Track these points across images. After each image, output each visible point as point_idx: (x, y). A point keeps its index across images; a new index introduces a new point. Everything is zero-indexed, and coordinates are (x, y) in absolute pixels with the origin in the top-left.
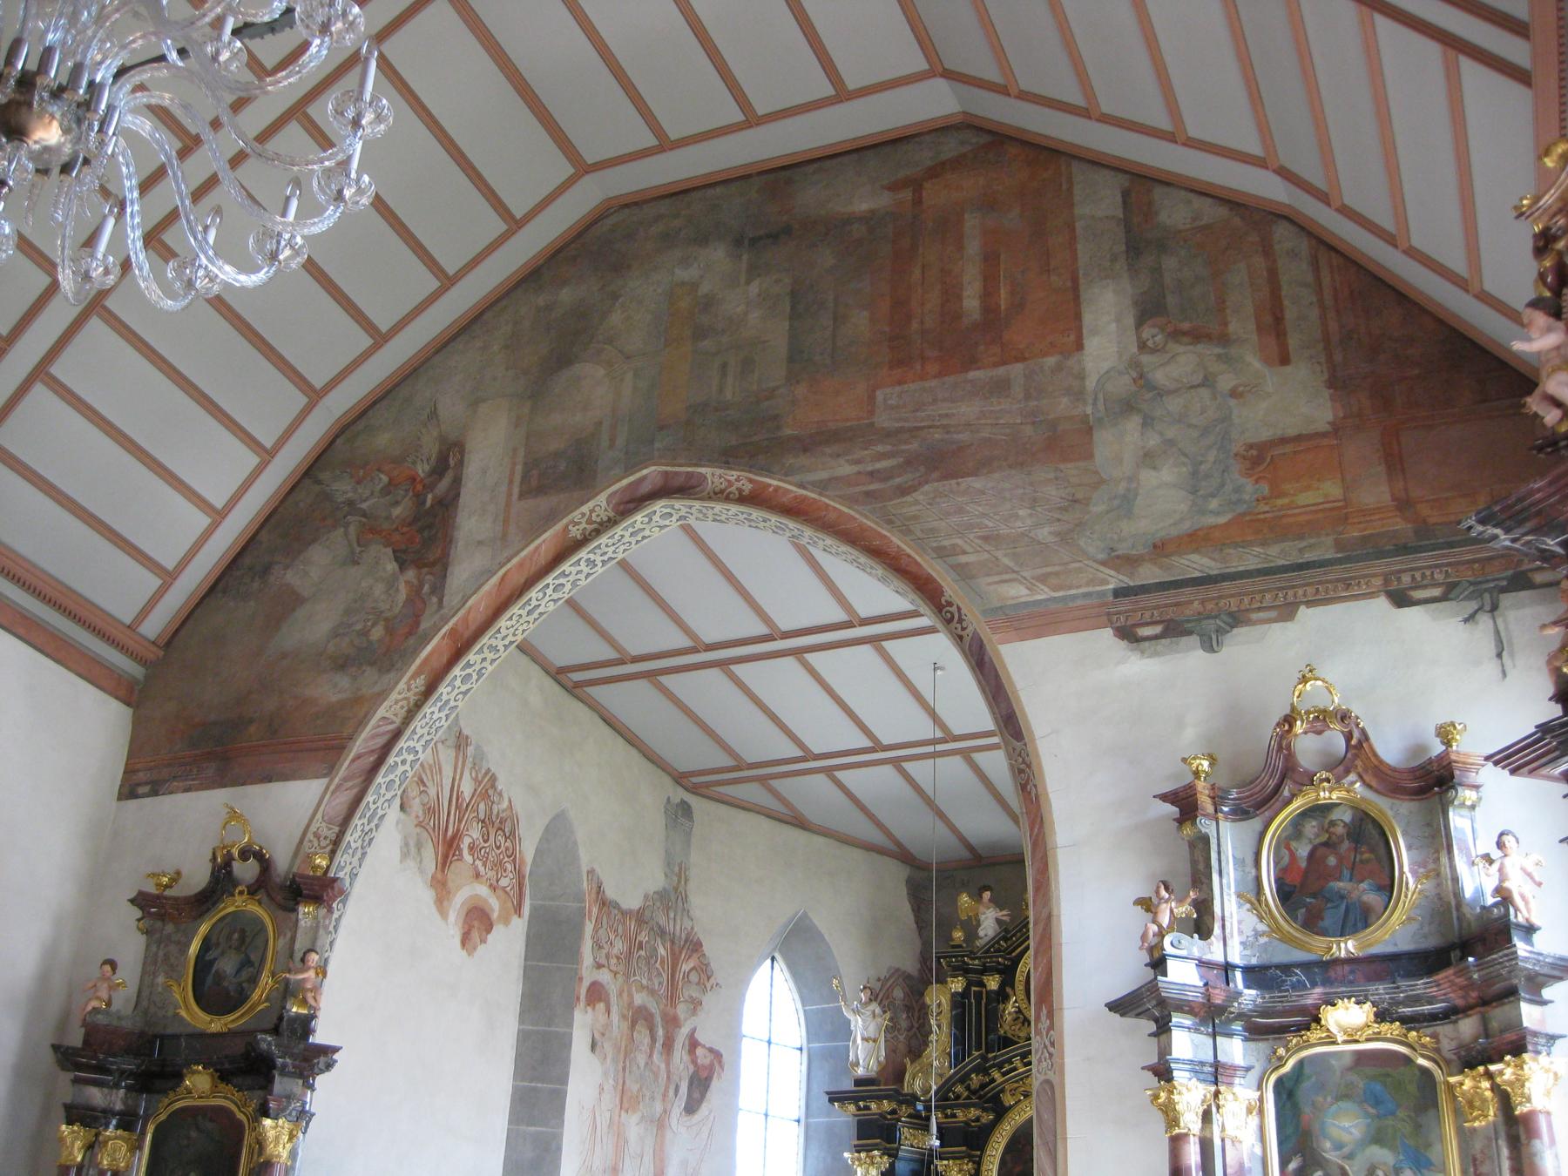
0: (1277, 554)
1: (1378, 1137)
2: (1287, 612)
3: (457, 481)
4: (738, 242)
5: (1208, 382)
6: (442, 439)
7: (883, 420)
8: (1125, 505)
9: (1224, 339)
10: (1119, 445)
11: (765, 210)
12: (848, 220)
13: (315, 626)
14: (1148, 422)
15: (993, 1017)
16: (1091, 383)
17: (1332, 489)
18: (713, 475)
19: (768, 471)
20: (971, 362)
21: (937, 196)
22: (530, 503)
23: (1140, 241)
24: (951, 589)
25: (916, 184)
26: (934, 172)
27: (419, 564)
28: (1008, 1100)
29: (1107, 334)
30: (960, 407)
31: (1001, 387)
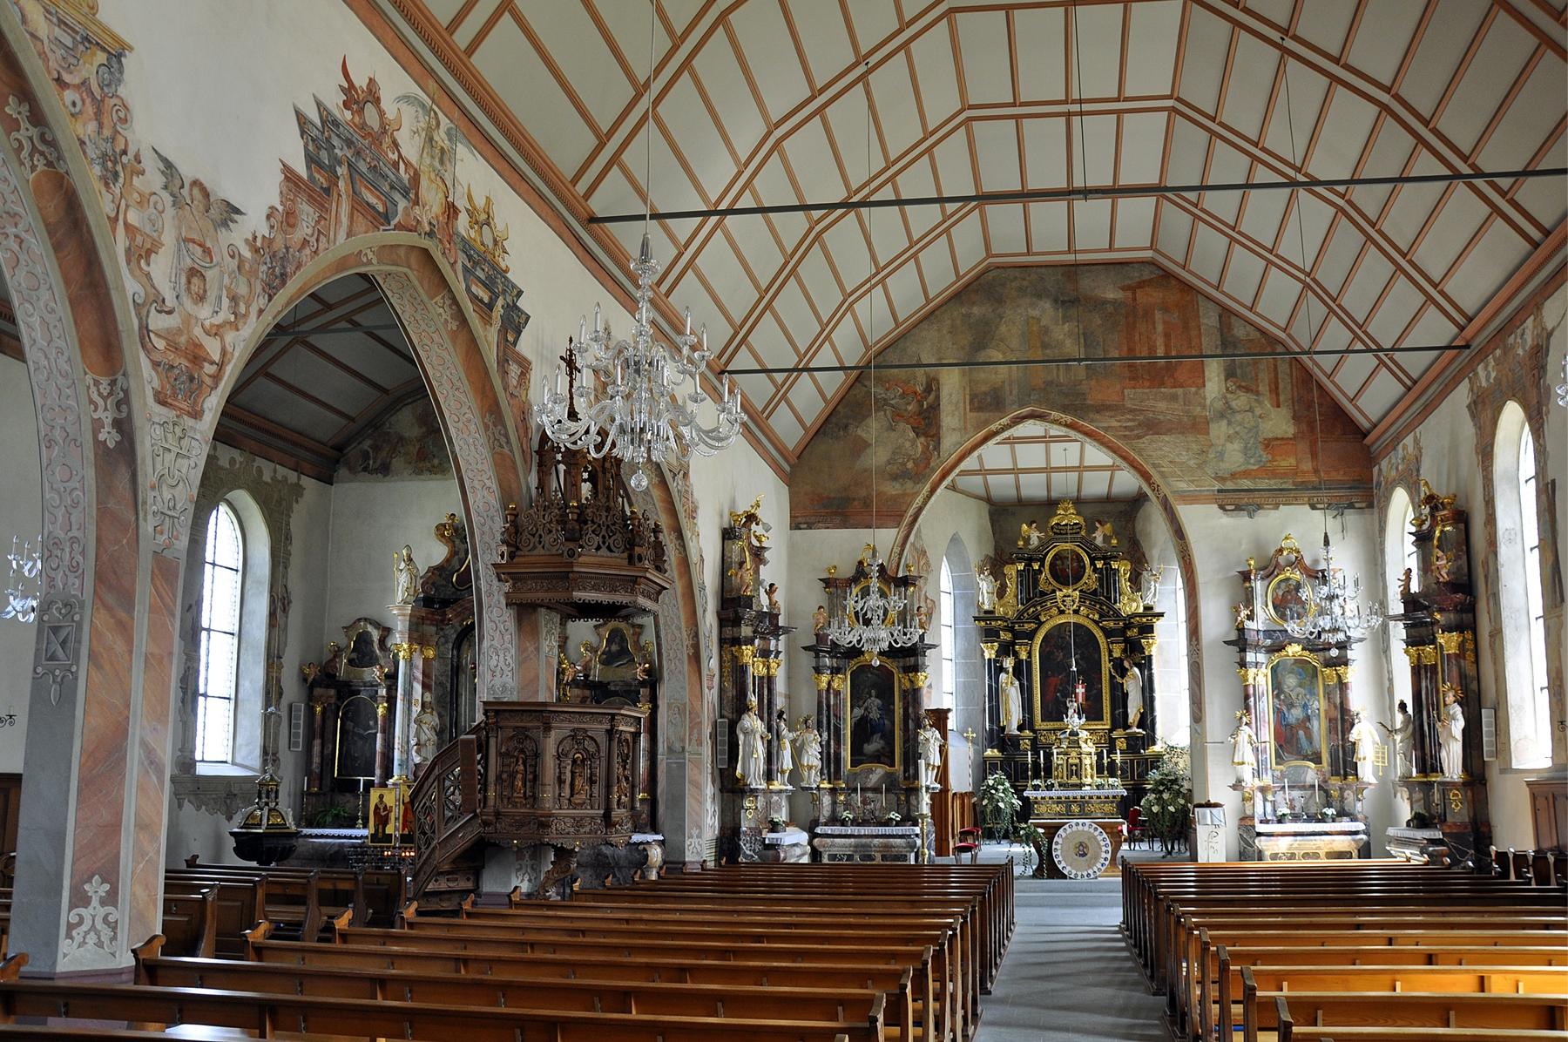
2: (1276, 507)
3: (938, 398)
4: (1056, 301)
5: (1251, 410)
7: (1128, 404)
8: (1221, 456)
9: (1257, 393)
10: (1219, 430)
11: (1065, 282)
12: (1105, 302)
13: (877, 457)
14: (1229, 423)
15: (1036, 582)
17: (1292, 461)
18: (1055, 414)
19: (1082, 418)
20: (1162, 384)
23: (1228, 346)
24: (1156, 478)
25: (1132, 289)
26: (1141, 284)
27: (926, 435)
30: (1160, 405)
31: (1174, 398)
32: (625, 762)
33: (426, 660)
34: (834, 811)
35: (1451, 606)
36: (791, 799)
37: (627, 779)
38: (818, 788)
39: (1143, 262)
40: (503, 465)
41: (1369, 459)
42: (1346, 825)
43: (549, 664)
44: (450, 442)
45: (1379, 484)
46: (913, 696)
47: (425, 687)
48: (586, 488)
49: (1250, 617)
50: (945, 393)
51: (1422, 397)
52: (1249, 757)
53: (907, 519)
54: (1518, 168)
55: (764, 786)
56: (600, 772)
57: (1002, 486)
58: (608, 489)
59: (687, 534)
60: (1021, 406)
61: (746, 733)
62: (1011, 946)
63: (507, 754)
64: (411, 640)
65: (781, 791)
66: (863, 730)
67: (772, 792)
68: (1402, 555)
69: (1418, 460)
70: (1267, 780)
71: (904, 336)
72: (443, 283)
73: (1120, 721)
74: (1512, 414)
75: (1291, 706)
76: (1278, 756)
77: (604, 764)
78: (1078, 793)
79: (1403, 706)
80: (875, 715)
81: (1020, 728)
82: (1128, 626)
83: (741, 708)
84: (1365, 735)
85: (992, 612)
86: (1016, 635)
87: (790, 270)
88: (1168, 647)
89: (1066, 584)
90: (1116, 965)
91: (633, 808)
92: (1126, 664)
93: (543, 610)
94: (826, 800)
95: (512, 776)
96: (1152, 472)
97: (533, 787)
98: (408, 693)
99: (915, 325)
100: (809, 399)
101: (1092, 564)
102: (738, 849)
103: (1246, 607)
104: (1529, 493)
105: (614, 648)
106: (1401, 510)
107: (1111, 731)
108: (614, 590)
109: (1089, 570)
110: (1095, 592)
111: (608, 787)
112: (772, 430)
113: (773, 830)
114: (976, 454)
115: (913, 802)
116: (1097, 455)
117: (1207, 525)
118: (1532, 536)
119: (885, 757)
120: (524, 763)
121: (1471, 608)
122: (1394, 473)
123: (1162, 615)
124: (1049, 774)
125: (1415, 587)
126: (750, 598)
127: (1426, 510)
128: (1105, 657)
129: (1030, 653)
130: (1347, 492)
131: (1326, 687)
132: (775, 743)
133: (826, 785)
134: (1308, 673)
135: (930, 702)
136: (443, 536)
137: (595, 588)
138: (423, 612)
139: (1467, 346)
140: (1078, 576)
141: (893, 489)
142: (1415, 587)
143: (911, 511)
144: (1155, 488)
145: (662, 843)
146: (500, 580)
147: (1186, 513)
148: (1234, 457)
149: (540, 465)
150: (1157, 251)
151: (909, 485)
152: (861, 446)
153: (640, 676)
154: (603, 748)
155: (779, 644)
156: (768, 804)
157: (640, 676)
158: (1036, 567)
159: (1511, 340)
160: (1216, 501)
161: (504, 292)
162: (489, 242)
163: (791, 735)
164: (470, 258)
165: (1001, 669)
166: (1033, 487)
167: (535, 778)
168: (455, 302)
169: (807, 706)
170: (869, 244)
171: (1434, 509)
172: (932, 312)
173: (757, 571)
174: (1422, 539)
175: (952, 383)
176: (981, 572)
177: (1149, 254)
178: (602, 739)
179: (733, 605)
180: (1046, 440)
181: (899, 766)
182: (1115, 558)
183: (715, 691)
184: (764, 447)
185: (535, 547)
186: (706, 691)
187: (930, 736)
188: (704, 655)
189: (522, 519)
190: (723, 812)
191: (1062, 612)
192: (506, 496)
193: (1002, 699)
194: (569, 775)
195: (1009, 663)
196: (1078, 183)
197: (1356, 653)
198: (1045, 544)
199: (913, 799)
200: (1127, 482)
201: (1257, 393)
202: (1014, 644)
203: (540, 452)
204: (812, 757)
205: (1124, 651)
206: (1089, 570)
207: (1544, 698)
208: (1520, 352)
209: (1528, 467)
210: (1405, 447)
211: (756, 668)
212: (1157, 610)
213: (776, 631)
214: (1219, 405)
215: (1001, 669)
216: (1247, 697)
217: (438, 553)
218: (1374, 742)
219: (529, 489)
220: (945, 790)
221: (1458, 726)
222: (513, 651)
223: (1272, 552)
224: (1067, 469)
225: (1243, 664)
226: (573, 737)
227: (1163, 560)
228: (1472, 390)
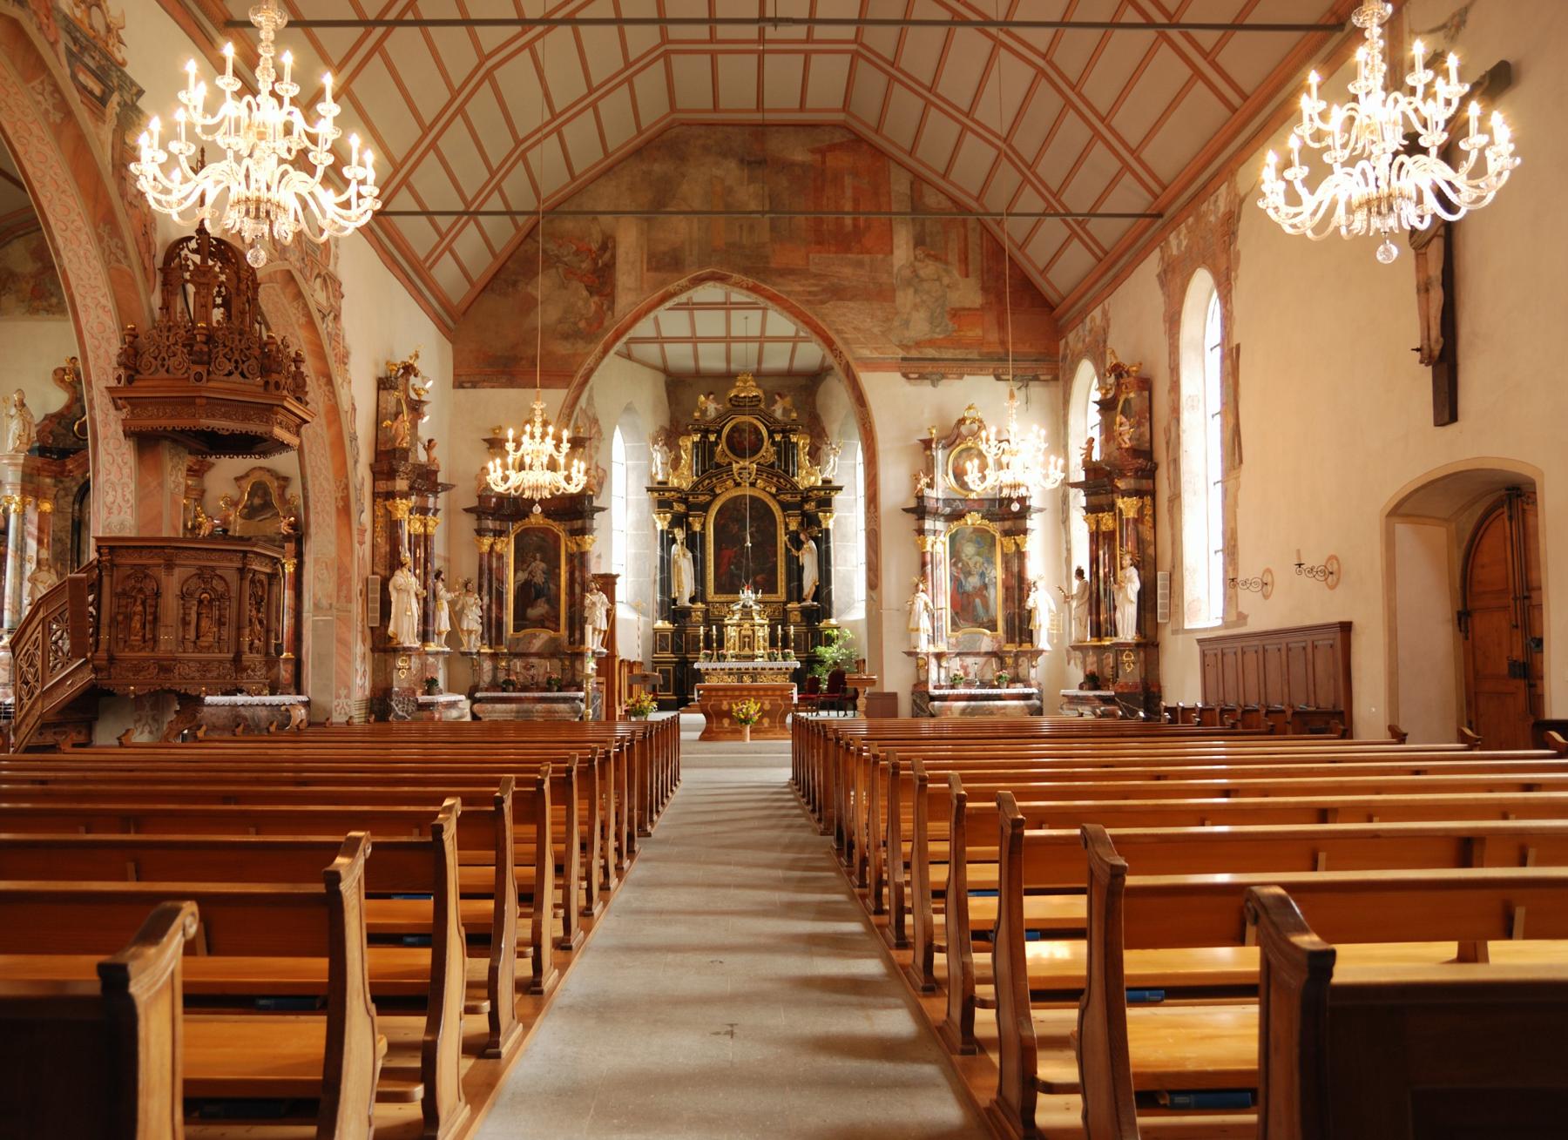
0: (959, 354)
1: (978, 554)
2: (961, 376)
3: (613, 256)
4: (742, 161)
5: (939, 279)
6: (603, 233)
7: (813, 269)
8: (906, 323)
9: (946, 263)
10: (905, 298)
11: (752, 142)
12: (793, 164)
13: (545, 316)
14: (916, 291)
15: (712, 453)
16: (895, 269)
17: (978, 332)
18: (736, 277)
19: (764, 281)
20: (848, 250)
21: (831, 160)
22: (652, 274)
23: (916, 207)
24: (839, 344)
25: (822, 152)
26: (832, 147)
27: (600, 293)
28: (718, 491)
29: (902, 251)
30: (845, 270)
31: (860, 264)
32: (259, 604)
33: (42, 515)
34: (495, 676)
35: (1129, 479)
36: (449, 660)
37: (261, 622)
38: (478, 653)
39: (835, 126)
40: (119, 282)
41: (1057, 331)
42: (1019, 689)
43: (175, 502)
44: (68, 287)
45: (1065, 357)
46: (579, 560)
47: (40, 542)
48: (217, 314)
49: (930, 486)
50: (621, 252)
51: (1112, 268)
52: (925, 623)
53: (577, 380)
54: (1228, 21)
55: (417, 644)
56: (230, 613)
57: (679, 356)
58: (243, 313)
59: (338, 380)
60: (701, 267)
61: (398, 590)
62: (678, 795)
63: (124, 594)
64: (24, 492)
65: (437, 653)
66: (527, 594)
67: (427, 654)
68: (1086, 421)
69: (1105, 331)
70: (942, 647)
71: (581, 187)
72: (40, 66)
73: (796, 592)
74: (1202, 281)
75: (969, 574)
76: (954, 623)
77: (234, 604)
78: (750, 665)
79: (1080, 573)
80: (539, 579)
81: (693, 600)
82: (806, 499)
83: (395, 563)
84: (1043, 603)
85: (665, 483)
86: (690, 507)
87: (457, 106)
88: (847, 522)
89: (742, 456)
90: (786, 822)
91: (267, 653)
92: (802, 537)
93: (167, 443)
94: (487, 665)
95: (128, 618)
96: (835, 337)
97: (154, 630)
98: (21, 548)
99: (592, 181)
100: (473, 249)
101: (771, 436)
102: (389, 710)
103: (926, 475)
104: (1214, 359)
105: (257, 501)
106: (1087, 386)
107: (785, 603)
108: (247, 419)
109: (767, 443)
110: (772, 466)
111: (239, 629)
112: (435, 283)
113: (428, 693)
114: (652, 315)
115: (578, 666)
116: (781, 324)
117: (888, 393)
118: (1215, 401)
119: (550, 621)
120: (143, 603)
121: (1150, 472)
122: (1080, 345)
123: (840, 488)
124: (721, 645)
125: (1096, 456)
126: (406, 451)
127: (1111, 380)
128: (781, 531)
129: (704, 526)
130: (1034, 365)
131: (1004, 555)
132: (431, 605)
133: (486, 650)
134: (984, 540)
135: (596, 568)
136: (62, 381)
137: (226, 416)
138: (39, 462)
139: (1160, 215)
140: (756, 448)
141: (562, 348)
142: (1096, 456)
143: (582, 372)
144: (838, 354)
145: (307, 704)
146: (117, 408)
147: (868, 380)
148: (920, 326)
149: (165, 283)
150: (849, 113)
151: (580, 345)
152: (529, 304)
153: (284, 528)
154: (234, 587)
155: (441, 500)
156: (424, 666)
157: (284, 528)
158: (712, 438)
159: (1204, 207)
160: (898, 369)
161: (121, 88)
162: (99, 25)
163: (450, 596)
164: (75, 41)
165: (674, 541)
166: (712, 359)
167: (156, 619)
168: (57, 89)
169: (468, 568)
170: (547, 95)
171: (1119, 376)
172: (610, 168)
173: (414, 426)
174: (1106, 406)
175: (629, 239)
176: (655, 442)
177: (841, 117)
178: (232, 577)
179: (387, 460)
180: (727, 306)
181: (564, 632)
182: (794, 431)
183: (367, 547)
184: (426, 300)
185: (157, 370)
186: (357, 545)
187: (596, 601)
188: (354, 508)
189: (142, 339)
190: (374, 672)
191: (738, 485)
192: (123, 310)
193: (674, 571)
194: (194, 616)
195: (680, 534)
196: (770, 13)
197: (1034, 522)
198: (722, 417)
199: (578, 665)
200: (811, 354)
201: (946, 263)
202: (687, 515)
203: (166, 269)
204: (473, 620)
205: (801, 524)
206: (767, 443)
207: (1218, 561)
208: (1212, 218)
209: (1214, 333)
210: (1093, 320)
211: (411, 526)
212: (836, 484)
213: (434, 488)
214: (907, 273)
215: (674, 541)
216: (924, 565)
217: (57, 399)
218: (1050, 611)
219: (151, 310)
220: (612, 656)
221: (1133, 586)
222: (132, 486)
223: (955, 421)
224: (747, 339)
225: (921, 532)
226: (199, 576)
227: (843, 434)
228: (1162, 258)
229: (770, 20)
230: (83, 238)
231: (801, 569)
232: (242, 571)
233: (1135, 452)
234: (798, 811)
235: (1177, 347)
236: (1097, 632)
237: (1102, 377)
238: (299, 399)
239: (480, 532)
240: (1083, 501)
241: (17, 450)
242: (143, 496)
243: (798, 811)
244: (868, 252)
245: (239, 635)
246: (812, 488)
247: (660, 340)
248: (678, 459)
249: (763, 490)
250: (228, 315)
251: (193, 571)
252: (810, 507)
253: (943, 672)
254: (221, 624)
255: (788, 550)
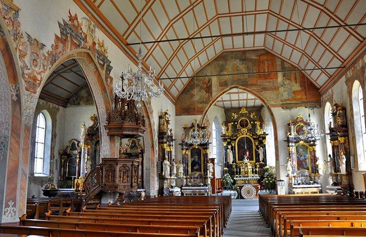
3: (211, 83)
5: (290, 84)
9: (291, 80)
10: (282, 89)
12: (253, 59)
13: (197, 98)
15: (236, 127)
23: (283, 69)
24: (266, 101)
25: (259, 56)
26: (261, 55)
30: (266, 83)
41: (320, 95)
43: (117, 149)
45: (323, 101)
46: (206, 155)
47: (88, 155)
48: (126, 107)
50: (213, 82)
53: (204, 113)
54: (357, 23)
55: (169, 177)
57: (227, 104)
59: (151, 117)
68: (329, 119)
70: (295, 174)
71: (203, 69)
73: (258, 160)
78: (247, 178)
80: (196, 160)
81: (233, 162)
82: (259, 137)
83: (164, 159)
84: (320, 163)
88: (270, 142)
89: (244, 128)
91: (138, 183)
94: (185, 181)
95: (109, 176)
98: (84, 157)
100: (180, 85)
101: (250, 122)
106: (328, 107)
110: (251, 129)
116: (251, 96)
123: (268, 134)
124: (240, 174)
128: (254, 145)
129: (235, 145)
131: (310, 151)
135: (210, 157)
137: (129, 131)
140: (247, 125)
141: (200, 106)
145: (145, 191)
149: (115, 102)
156: (170, 182)
157: (140, 151)
163: (176, 165)
165: (228, 148)
166: (235, 104)
169: (180, 158)
171: (337, 107)
174: (334, 114)
175: (215, 80)
177: (263, 47)
178: (130, 167)
180: (238, 93)
181: (202, 172)
182: (256, 121)
183: (157, 155)
187: (210, 165)
188: (155, 146)
191: (243, 134)
195: (230, 147)
196: (245, 31)
197: (318, 143)
198: (238, 118)
200: (259, 102)
201: (291, 80)
204: (181, 170)
206: (249, 124)
208: (358, 68)
211: (167, 149)
212: (266, 133)
213: (172, 140)
216: (290, 154)
217: (91, 123)
220: (214, 178)
224: (243, 100)
225: (289, 146)
229: (245, 33)
230: (99, 94)
231: (259, 154)
232: (132, 165)
233: (342, 126)
234: (261, 220)
235: (352, 100)
236: (335, 171)
237: (332, 106)
238: (144, 126)
239: (182, 149)
240: (330, 138)
241: (83, 135)
242: (111, 148)
243: (261, 220)
244: (272, 79)
245: (132, 179)
246: (261, 135)
247: (223, 101)
248: (228, 128)
249: (249, 136)
250: (128, 108)
251: (122, 165)
252: (261, 139)
253: (296, 181)
254: (128, 177)
255: (256, 150)
